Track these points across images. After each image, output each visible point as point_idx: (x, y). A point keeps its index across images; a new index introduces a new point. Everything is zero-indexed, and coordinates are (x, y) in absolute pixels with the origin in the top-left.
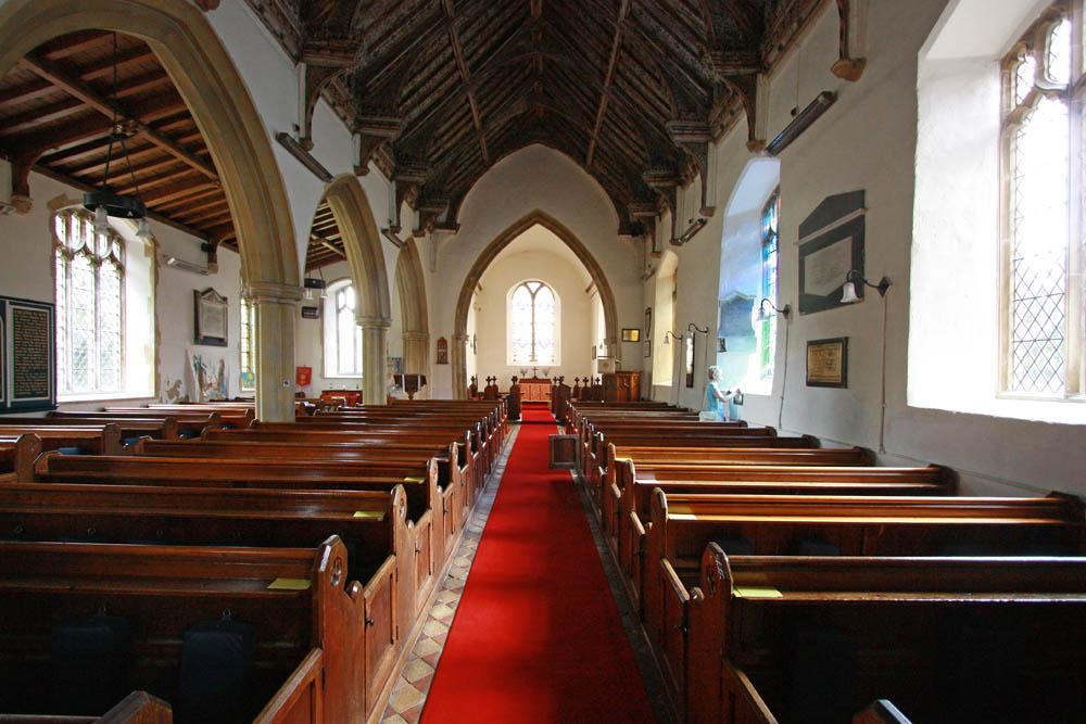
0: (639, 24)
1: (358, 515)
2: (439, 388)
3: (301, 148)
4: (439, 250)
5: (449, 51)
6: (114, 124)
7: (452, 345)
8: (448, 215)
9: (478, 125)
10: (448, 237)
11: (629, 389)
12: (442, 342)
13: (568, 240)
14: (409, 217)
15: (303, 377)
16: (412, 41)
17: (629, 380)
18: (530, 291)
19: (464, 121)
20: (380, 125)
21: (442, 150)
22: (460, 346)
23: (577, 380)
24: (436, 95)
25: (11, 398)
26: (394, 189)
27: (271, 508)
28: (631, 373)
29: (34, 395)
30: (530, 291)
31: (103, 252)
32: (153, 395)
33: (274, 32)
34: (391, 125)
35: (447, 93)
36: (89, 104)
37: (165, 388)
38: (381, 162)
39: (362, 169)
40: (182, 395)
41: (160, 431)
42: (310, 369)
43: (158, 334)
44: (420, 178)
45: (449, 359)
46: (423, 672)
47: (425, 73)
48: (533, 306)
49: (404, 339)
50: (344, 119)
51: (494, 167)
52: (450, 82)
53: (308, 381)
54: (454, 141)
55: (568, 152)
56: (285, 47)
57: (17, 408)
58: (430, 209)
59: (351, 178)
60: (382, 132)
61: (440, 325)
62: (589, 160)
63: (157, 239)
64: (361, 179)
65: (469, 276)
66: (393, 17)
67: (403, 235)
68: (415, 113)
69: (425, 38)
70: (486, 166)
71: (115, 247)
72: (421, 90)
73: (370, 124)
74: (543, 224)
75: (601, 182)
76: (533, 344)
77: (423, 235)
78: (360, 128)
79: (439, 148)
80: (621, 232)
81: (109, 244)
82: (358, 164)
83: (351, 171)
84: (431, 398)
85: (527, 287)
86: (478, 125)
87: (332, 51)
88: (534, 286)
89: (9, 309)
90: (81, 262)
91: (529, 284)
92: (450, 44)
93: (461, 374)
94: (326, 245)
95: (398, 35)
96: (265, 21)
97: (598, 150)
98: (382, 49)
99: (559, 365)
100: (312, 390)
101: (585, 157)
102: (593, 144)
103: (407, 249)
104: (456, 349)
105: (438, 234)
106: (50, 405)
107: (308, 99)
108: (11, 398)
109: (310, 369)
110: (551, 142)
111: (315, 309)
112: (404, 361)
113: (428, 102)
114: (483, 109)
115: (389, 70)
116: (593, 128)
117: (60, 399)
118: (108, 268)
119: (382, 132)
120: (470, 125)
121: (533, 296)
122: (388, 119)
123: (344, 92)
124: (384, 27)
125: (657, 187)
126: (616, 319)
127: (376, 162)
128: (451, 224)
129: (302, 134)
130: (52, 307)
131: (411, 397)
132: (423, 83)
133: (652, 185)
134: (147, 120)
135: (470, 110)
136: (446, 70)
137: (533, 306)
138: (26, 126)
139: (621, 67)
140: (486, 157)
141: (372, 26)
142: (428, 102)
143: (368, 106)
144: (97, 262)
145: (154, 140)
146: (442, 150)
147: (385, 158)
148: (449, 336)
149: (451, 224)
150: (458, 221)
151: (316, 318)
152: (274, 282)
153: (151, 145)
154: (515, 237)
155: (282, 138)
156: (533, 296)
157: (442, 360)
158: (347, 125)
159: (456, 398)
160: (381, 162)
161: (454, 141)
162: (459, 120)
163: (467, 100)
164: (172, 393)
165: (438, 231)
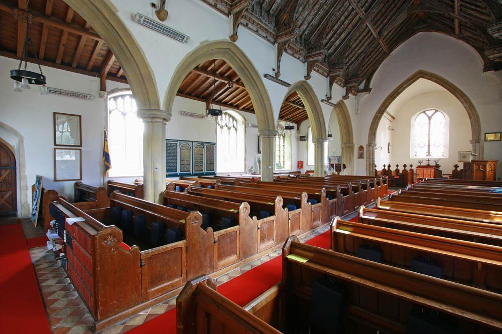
1: (231, 210)
2: (357, 169)
3: (276, 78)
4: (360, 103)
5: (351, 7)
6: (226, 84)
7: (367, 149)
8: (365, 85)
9: (376, 36)
10: (365, 96)
11: (484, 172)
12: (361, 148)
13: (440, 82)
14: (338, 91)
15: (300, 165)
16: (329, 12)
17: (485, 167)
18: (427, 115)
19: (367, 37)
20: (315, 55)
21: (356, 55)
22: (371, 149)
23: (384, 166)
24: (347, 31)
25: (205, 171)
26: (329, 81)
27: (214, 205)
28: (487, 161)
29: (211, 170)
30: (427, 115)
31: (231, 125)
32: (244, 171)
33: (263, 37)
34: (319, 54)
35: (353, 27)
36: (220, 81)
37: (248, 169)
38: (320, 71)
39: (308, 77)
40: (253, 172)
41: (234, 183)
42: (303, 162)
43: (246, 151)
44: (341, 73)
45: (365, 156)
46: (248, 268)
48: (429, 124)
49: (342, 147)
50: (299, 58)
51: (392, 53)
52: (354, 21)
53: (302, 167)
54: (363, 48)
55: (443, 31)
56: (268, 40)
57: (207, 174)
58: (351, 85)
59: (304, 82)
60: (315, 59)
61: (360, 139)
62: (457, 32)
63: (246, 118)
64: (308, 81)
65: (377, 113)
66: (317, 6)
67: (334, 101)
68: (337, 43)
69: (335, 8)
70: (386, 55)
71: (235, 122)
72: (338, 32)
73: (310, 56)
74: (423, 77)
75: (468, 42)
76: (429, 146)
77: (348, 98)
78: (307, 59)
79: (355, 54)
80: (486, 69)
81: (233, 122)
82: (306, 75)
83: (303, 79)
84: (355, 175)
85: (426, 114)
86: (376, 36)
87: (286, 35)
88: (430, 113)
89: (205, 145)
90: (225, 129)
91: (426, 112)
92: (350, 5)
93: (372, 164)
95: (321, 13)
96: (259, 35)
97: (462, 27)
98: (315, 22)
99: (447, 157)
100: (303, 170)
101: (453, 29)
102: (456, 21)
103: (340, 106)
104: (368, 151)
105: (359, 95)
106: (214, 174)
107: (278, 57)
108: (205, 171)
109: (303, 162)
110: (429, 28)
111: (305, 137)
112: (342, 158)
113: (343, 36)
114: (376, 29)
115: (318, 30)
116: (454, 12)
117: (217, 172)
118: (233, 129)
119: (315, 59)
120: (372, 37)
121: (430, 118)
122: (318, 52)
123: (297, 47)
124: (313, 13)
126: (479, 126)
127: (318, 71)
128: (367, 89)
130: (215, 144)
131: (338, 174)
132: (339, 28)
134: (235, 80)
135: (369, 30)
137: (429, 124)
138: (208, 91)
140: (386, 50)
141: (308, 15)
142: (343, 36)
143: (309, 49)
144: (229, 128)
145: (239, 86)
146: (356, 55)
147: (322, 68)
148: (364, 144)
149: (367, 89)
150: (371, 87)
151: (305, 140)
152: (266, 130)
153: (238, 88)
154: (405, 88)
155: (266, 76)
156: (430, 118)
157: (361, 156)
158: (301, 61)
159: (368, 175)
160: (320, 71)
161: (363, 48)
162: (365, 37)
163: (367, 26)
164: (250, 170)
165: (360, 94)
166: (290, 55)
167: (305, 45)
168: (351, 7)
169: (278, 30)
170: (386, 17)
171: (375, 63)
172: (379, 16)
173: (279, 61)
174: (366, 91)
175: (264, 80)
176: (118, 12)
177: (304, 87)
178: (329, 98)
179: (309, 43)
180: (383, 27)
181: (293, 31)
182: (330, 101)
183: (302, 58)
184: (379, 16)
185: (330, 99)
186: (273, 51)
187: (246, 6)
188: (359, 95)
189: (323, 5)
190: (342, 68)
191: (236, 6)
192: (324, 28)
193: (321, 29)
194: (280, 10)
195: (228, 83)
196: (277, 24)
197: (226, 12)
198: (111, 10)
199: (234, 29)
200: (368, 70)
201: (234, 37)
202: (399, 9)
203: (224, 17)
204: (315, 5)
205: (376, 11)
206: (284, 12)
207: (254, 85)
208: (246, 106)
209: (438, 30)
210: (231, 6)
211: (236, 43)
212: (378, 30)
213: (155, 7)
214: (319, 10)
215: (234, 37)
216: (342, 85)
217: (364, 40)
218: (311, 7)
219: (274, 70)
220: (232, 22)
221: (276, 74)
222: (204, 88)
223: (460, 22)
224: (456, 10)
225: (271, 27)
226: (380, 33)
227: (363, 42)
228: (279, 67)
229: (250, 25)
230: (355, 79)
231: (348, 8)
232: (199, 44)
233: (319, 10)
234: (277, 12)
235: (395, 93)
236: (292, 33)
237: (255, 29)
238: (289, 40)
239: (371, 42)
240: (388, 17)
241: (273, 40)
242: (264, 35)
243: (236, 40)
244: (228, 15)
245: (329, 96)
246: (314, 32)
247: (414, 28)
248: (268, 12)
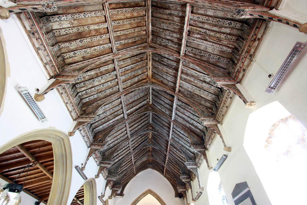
0: (174, 140)
3: (81, 170)
5: (128, 145)
16: (119, 143)
20: (106, 163)
21: (122, 171)
24: (123, 156)
34: (109, 164)
35: (126, 155)
47: (121, 150)
51: (137, 175)
52: (127, 153)
55: (159, 171)
60: (106, 166)
64: (96, 179)
67: (105, 199)
68: (117, 160)
69: (122, 143)
72: (119, 155)
73: (103, 163)
74: (151, 194)
83: (94, 177)
87: (98, 145)
94: (78, 202)
95: (116, 142)
98: (111, 145)
105: (117, 198)
110: (153, 168)
119: (106, 166)
120: (131, 163)
122: (109, 162)
123: (98, 155)
124: (113, 140)
125: (186, 181)
128: (121, 194)
129: (83, 166)
133: (183, 180)
135: (132, 159)
136: (127, 150)
139: (171, 149)
140: (135, 173)
141: (110, 140)
146: (122, 171)
149: (121, 194)
158: (97, 163)
163: (131, 157)
165: (117, 196)
166: (93, 158)
167: (102, 155)
168: (128, 145)
169: (94, 141)
170: (139, 156)
171: (129, 178)
172: (137, 154)
173: (88, 159)
174: (121, 196)
175: (74, 170)
176: (10, 77)
177: (91, 184)
178: (103, 196)
179: (104, 155)
180: (137, 160)
181: (104, 145)
182: (103, 198)
183: (98, 162)
184: (137, 154)
185: (103, 197)
186: (87, 151)
187: (89, 122)
188: (117, 198)
189: (118, 139)
190: (116, 176)
191: (82, 119)
192: (115, 150)
193: (114, 149)
194: (99, 131)
195: (33, 162)
196: (95, 137)
197: (74, 118)
198: (5, 76)
199: (74, 129)
200: (124, 181)
201: (71, 134)
202: (144, 154)
203: (72, 120)
204: (115, 137)
205: (137, 151)
206: (101, 134)
207: (65, 171)
208: (28, 188)
209: (157, 170)
210: (79, 117)
211: (70, 138)
212: (135, 160)
213: (38, 91)
214: (116, 140)
215: (71, 134)
216: (111, 188)
217: (128, 164)
218: (113, 137)
219: (82, 164)
220: (74, 125)
221: (82, 168)
222: (3, 159)
223: (166, 169)
224: (166, 164)
225: (91, 138)
226: (135, 162)
227: (127, 164)
228: (86, 163)
229: (82, 132)
230: (119, 186)
231: (127, 145)
232: (48, 127)
233: (116, 140)
234: (97, 132)
235: (136, 201)
236: (103, 146)
237: (83, 135)
238: (99, 149)
239: (130, 166)
240: (140, 157)
241: (89, 145)
242: (86, 140)
243: (73, 135)
244: (74, 120)
245: (103, 194)
246: (109, 150)
247: (148, 165)
248: (93, 129)
